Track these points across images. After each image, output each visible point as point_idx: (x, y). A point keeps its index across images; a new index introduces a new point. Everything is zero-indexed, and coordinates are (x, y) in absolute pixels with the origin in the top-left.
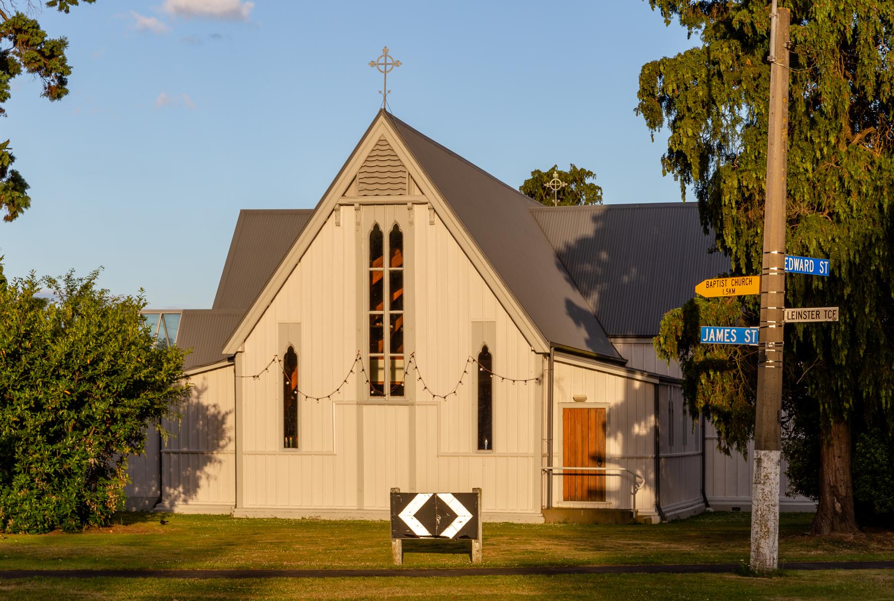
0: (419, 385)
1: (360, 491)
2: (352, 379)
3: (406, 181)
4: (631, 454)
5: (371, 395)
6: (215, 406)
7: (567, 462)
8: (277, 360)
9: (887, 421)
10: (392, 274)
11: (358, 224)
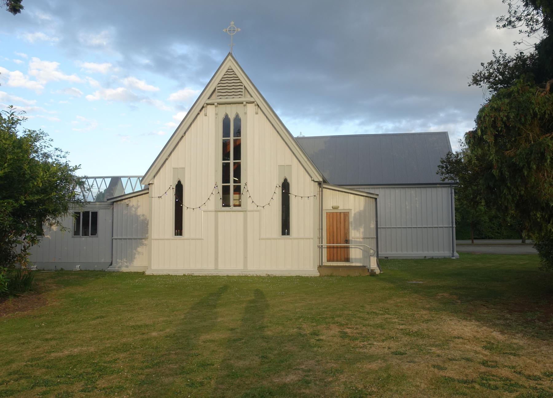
0: (249, 201)
1: (216, 259)
2: (212, 198)
3: (243, 90)
4: (367, 236)
5: (223, 206)
6: (143, 215)
7: (329, 241)
8: (171, 188)
9: (124, 270)
10: (235, 141)
11: (216, 114)
